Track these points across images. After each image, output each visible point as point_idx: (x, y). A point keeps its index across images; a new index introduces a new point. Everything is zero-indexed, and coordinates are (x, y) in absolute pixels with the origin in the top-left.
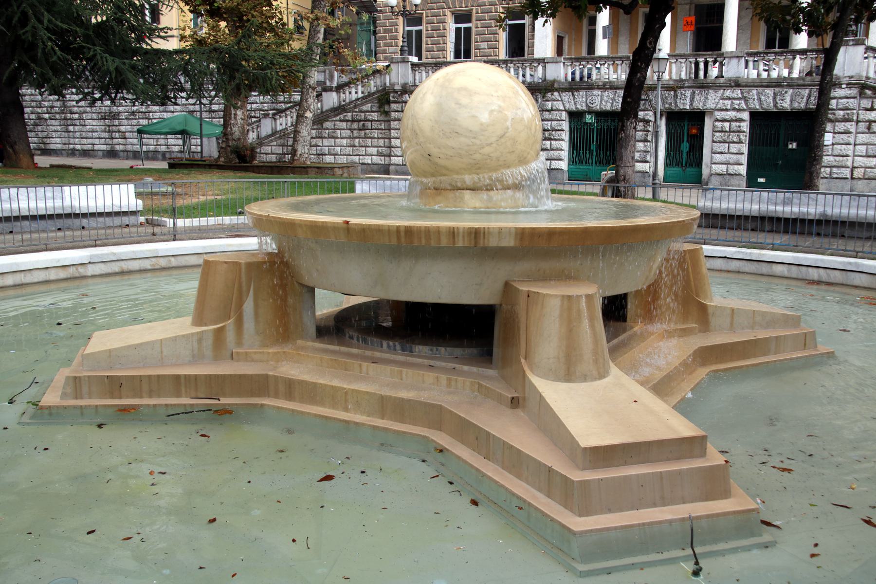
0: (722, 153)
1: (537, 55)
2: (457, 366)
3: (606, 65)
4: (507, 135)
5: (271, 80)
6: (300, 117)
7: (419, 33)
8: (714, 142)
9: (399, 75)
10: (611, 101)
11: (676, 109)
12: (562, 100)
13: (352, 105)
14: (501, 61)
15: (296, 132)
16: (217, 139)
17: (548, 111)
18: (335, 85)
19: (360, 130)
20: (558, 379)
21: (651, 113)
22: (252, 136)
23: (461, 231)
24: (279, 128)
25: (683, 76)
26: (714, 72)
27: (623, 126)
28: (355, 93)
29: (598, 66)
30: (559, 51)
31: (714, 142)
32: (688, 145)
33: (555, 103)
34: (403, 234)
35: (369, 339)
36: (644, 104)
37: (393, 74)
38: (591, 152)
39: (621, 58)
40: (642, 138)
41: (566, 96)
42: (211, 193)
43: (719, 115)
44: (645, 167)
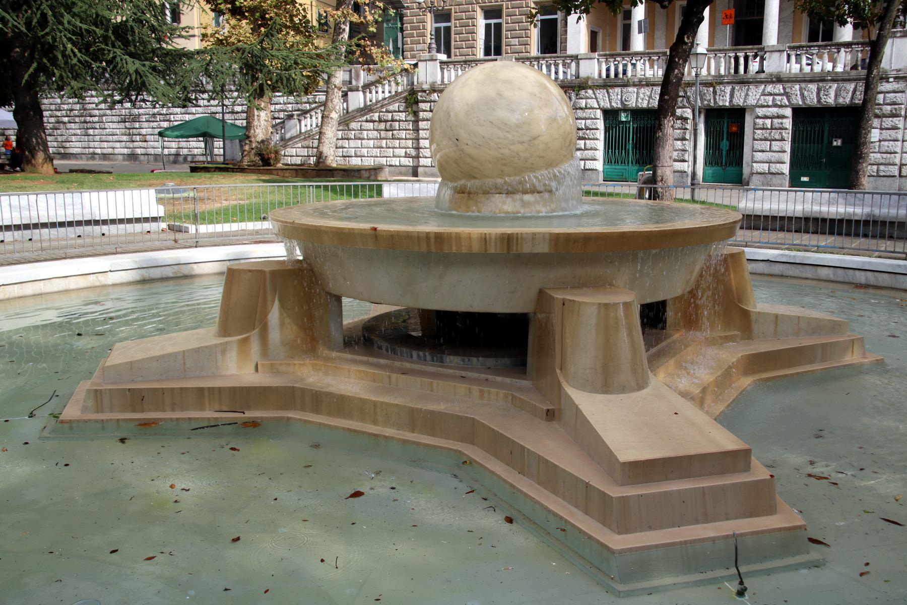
0: (763, 151)
1: (570, 51)
2: (490, 377)
8: (754, 139)
10: (647, 98)
12: (596, 98)
17: (581, 109)
18: (361, 84)
19: (387, 130)
20: (597, 392)
21: (689, 111)
23: (493, 237)
26: (754, 66)
29: (634, 62)
30: (593, 47)
32: (728, 143)
33: (589, 101)
35: (398, 349)
40: (680, 137)
41: (601, 94)
43: (760, 112)
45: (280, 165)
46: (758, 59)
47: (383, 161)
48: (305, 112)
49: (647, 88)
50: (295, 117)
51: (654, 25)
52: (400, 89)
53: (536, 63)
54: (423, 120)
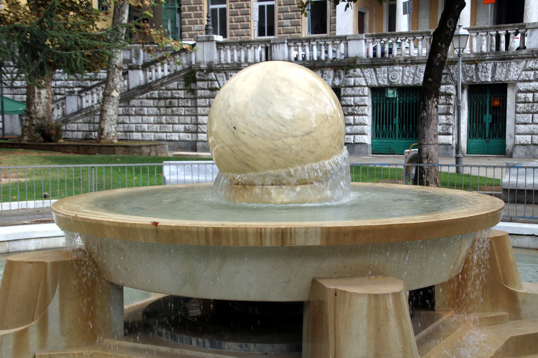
0: (525, 124)
1: (339, 33)
3: (407, 40)
4: (313, 134)
5: (75, 60)
6: (107, 96)
7: (223, 11)
8: (517, 113)
9: (205, 54)
10: (414, 76)
11: (478, 82)
12: (364, 77)
13: (159, 83)
14: (304, 39)
15: (103, 111)
16: (20, 116)
17: (350, 87)
18: (141, 62)
19: (167, 107)
21: (452, 87)
22: (57, 113)
23: (268, 231)
24: (85, 105)
25: (484, 49)
26: (516, 43)
27: (425, 105)
28: (161, 71)
29: (399, 41)
30: (361, 28)
31: (517, 113)
32: (490, 117)
33: (357, 79)
34: (211, 235)
35: (178, 336)
36: (446, 78)
37: (199, 53)
38: (394, 126)
39: (421, 34)
40: (445, 111)
41: (368, 72)
42: (14, 174)
43: (522, 86)
44: (449, 139)
45: (61, 141)
46: (519, 36)
47: (163, 136)
48: (86, 89)
49: (413, 66)
50: (76, 93)
51: (418, 5)
52: (179, 68)
53: (307, 44)
54: (201, 97)
